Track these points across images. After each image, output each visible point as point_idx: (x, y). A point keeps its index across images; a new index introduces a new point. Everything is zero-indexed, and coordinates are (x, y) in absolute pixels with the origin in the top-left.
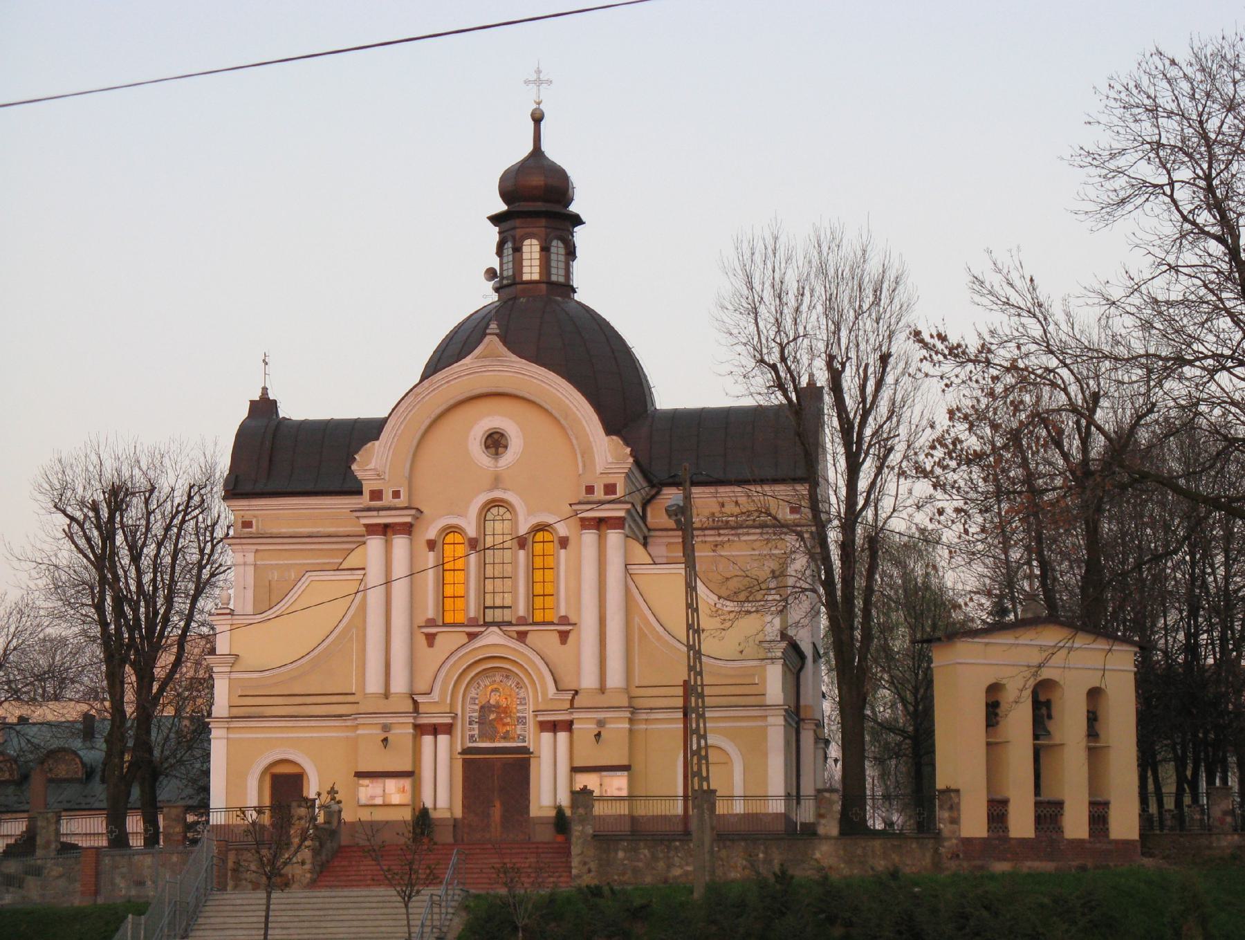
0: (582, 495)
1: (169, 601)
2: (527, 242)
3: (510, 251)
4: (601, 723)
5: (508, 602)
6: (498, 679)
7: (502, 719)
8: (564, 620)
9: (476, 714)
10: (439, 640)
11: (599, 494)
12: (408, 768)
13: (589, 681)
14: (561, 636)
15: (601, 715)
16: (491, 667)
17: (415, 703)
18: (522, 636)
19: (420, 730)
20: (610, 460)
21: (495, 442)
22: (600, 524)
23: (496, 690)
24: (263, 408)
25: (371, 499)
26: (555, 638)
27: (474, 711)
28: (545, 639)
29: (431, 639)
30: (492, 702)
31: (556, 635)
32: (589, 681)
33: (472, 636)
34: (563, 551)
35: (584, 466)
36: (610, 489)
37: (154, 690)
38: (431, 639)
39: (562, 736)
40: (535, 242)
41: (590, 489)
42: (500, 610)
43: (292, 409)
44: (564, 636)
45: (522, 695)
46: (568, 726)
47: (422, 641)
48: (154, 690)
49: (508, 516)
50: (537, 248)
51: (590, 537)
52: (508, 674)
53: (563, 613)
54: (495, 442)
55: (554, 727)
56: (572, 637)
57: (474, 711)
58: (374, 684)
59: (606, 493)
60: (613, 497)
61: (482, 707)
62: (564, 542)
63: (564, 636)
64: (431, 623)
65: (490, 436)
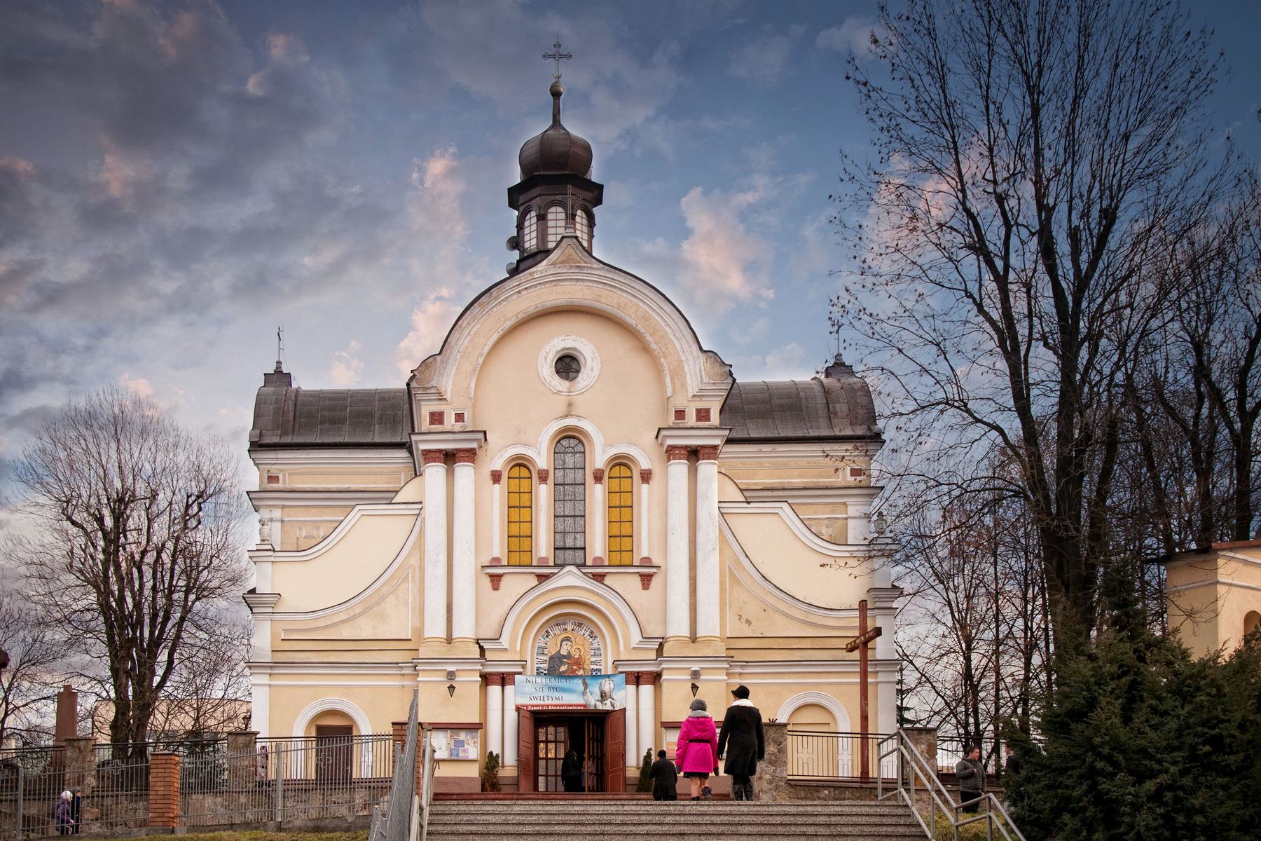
0: (671, 420)
1: (169, 597)
2: (553, 209)
3: (534, 220)
4: (696, 674)
5: (579, 544)
6: (569, 627)
7: (574, 671)
8: (647, 562)
9: (545, 666)
10: (505, 582)
11: (691, 419)
12: (476, 719)
13: (679, 627)
14: (643, 580)
15: (696, 667)
16: (568, 615)
17: (481, 648)
18: (599, 578)
19: (486, 679)
20: (706, 379)
21: (567, 365)
22: (694, 454)
23: (568, 639)
24: (279, 377)
25: (432, 423)
26: (637, 581)
27: (544, 662)
28: (627, 584)
29: (496, 580)
30: (564, 652)
31: (637, 580)
32: (679, 627)
33: (542, 578)
34: (645, 486)
35: (674, 389)
36: (703, 414)
37: (155, 684)
38: (496, 580)
39: (647, 690)
40: (560, 209)
41: (680, 414)
42: (571, 552)
43: (306, 381)
44: (646, 580)
45: (596, 646)
46: (655, 678)
47: (487, 582)
48: (155, 684)
49: (580, 448)
50: (563, 216)
51: (679, 468)
52: (581, 621)
53: (645, 554)
54: (567, 365)
55: (636, 679)
56: (655, 582)
57: (544, 662)
58: (435, 628)
59: (698, 419)
60: (706, 424)
61: (551, 658)
62: (646, 476)
63: (646, 580)
64: (495, 563)
65: (560, 359)
